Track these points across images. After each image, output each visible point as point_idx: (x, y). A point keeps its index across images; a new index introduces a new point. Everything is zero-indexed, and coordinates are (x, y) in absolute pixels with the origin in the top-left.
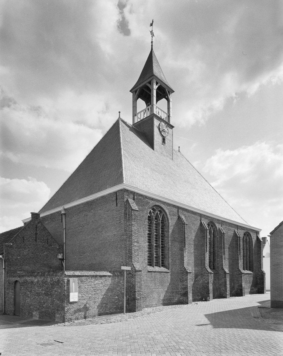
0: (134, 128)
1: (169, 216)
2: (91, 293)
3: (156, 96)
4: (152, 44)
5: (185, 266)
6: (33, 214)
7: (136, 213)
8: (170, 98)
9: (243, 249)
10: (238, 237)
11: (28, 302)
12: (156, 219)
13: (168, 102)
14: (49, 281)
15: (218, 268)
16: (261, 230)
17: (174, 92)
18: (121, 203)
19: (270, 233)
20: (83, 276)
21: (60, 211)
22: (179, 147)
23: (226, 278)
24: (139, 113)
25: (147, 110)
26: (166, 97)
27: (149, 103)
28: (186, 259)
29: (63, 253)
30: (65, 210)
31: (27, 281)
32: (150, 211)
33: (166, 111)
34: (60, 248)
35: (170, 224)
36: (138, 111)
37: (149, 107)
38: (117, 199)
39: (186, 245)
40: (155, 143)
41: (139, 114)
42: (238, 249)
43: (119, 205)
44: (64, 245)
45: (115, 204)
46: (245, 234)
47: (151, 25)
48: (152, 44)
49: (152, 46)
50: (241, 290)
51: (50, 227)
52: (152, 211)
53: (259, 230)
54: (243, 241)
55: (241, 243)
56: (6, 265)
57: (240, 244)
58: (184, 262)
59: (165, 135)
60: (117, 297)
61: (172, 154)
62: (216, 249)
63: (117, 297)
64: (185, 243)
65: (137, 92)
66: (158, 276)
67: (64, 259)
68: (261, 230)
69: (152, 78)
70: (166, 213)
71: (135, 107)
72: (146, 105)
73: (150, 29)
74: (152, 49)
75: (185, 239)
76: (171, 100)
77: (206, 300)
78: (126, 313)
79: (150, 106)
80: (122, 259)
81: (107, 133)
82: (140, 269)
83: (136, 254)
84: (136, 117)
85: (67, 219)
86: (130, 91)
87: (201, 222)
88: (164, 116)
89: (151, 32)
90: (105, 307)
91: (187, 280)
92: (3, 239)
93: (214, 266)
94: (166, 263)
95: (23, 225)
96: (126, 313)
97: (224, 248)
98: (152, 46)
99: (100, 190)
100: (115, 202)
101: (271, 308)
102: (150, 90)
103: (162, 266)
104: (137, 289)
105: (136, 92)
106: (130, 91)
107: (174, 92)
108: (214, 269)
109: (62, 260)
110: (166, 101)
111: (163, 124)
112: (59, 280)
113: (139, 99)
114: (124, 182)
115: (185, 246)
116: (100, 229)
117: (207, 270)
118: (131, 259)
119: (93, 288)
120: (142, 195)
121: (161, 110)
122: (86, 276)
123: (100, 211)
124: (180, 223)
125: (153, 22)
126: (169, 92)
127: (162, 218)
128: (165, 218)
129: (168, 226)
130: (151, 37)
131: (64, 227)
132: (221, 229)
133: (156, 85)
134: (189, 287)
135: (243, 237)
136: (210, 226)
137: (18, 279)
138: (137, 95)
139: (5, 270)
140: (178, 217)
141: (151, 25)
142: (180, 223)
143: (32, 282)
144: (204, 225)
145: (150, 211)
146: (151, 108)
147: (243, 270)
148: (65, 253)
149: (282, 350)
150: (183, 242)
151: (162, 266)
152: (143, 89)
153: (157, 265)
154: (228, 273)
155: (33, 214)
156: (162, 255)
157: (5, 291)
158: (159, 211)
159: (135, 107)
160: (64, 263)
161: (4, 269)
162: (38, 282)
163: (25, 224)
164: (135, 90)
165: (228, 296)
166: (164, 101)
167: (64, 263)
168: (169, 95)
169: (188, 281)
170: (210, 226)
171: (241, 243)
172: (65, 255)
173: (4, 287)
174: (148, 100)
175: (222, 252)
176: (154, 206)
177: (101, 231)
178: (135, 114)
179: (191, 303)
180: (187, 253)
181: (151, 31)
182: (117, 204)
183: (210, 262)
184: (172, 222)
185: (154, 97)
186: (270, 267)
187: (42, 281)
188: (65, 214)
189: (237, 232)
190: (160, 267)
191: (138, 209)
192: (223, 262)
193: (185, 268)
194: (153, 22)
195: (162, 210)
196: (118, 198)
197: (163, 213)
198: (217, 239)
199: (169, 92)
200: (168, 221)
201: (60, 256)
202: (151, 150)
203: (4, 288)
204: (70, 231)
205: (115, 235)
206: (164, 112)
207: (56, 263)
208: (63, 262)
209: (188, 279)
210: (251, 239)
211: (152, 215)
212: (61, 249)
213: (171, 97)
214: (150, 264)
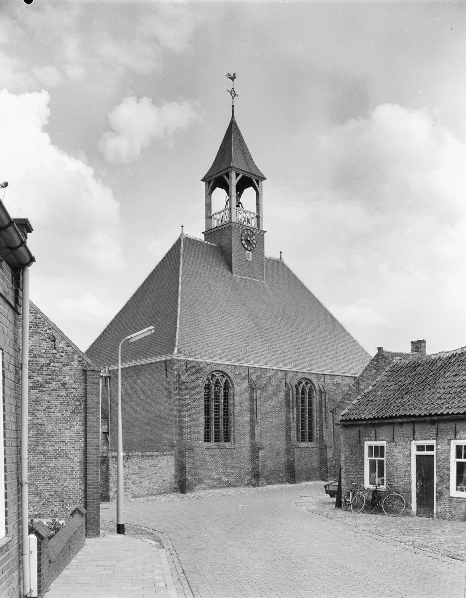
1: (233, 381)
4: (233, 109)
22: (281, 252)
36: (213, 212)
43: (169, 376)
48: (233, 109)
49: (233, 111)
71: (209, 206)
74: (233, 117)
98: (233, 111)
99: (378, 472)
105: (209, 182)
118: (182, 436)
126: (258, 182)
130: (232, 99)
149: (465, 501)
168: (259, 186)
176: (213, 372)
178: (209, 217)
188: (110, 377)
197: (226, 378)
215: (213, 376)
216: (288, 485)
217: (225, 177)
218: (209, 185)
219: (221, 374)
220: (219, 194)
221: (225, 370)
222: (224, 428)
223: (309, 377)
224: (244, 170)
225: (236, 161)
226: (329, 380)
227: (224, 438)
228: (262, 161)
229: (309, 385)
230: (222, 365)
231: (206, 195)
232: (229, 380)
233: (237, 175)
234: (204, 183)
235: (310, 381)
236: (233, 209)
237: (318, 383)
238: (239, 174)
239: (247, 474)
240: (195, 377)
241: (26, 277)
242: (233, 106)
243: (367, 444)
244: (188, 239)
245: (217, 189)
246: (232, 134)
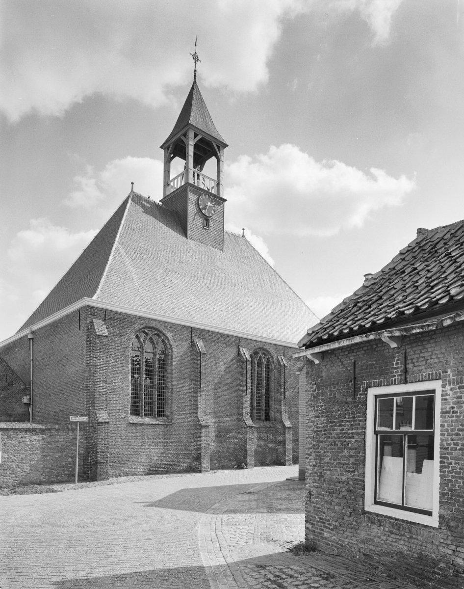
1: (172, 342)
2: (24, 453)
3: (193, 155)
4: (195, 74)
5: (199, 416)
7: (104, 340)
8: (220, 155)
13: (218, 162)
15: (275, 420)
17: (227, 146)
20: (12, 429)
21: (26, 336)
23: (285, 434)
28: (201, 406)
29: (30, 394)
30: (33, 332)
34: (27, 388)
35: (175, 354)
38: (80, 320)
40: (189, 228)
41: (172, 182)
44: (31, 383)
48: (195, 74)
49: (195, 76)
58: (197, 411)
59: (209, 214)
60: (70, 460)
61: (220, 240)
62: (272, 390)
63: (70, 460)
65: (170, 148)
66: (149, 430)
69: (186, 129)
70: (167, 338)
71: (167, 172)
75: (200, 375)
76: (222, 158)
77: (240, 467)
78: (78, 481)
80: (83, 406)
83: (104, 398)
84: (167, 189)
86: (161, 147)
90: (50, 472)
91: (200, 437)
94: (168, 412)
96: (78, 481)
97: (285, 388)
98: (195, 76)
104: (100, 448)
105: (168, 148)
107: (227, 146)
109: (28, 405)
115: (200, 386)
117: (245, 422)
118: (94, 406)
119: (27, 445)
120: (121, 313)
122: (16, 429)
124: (195, 354)
126: (219, 148)
129: (172, 357)
131: (32, 358)
134: (204, 447)
142: (195, 354)
148: (31, 395)
150: (197, 379)
153: (149, 414)
154: (289, 428)
164: (167, 145)
175: (281, 395)
178: (167, 184)
179: (207, 471)
181: (193, 53)
184: (178, 350)
185: (190, 157)
188: (33, 339)
191: (107, 335)
192: (283, 410)
199: (219, 148)
201: (25, 400)
204: (37, 363)
207: (20, 410)
209: (202, 435)
212: (26, 390)
213: (225, 154)
214: (135, 412)
217: (183, 138)
218: (168, 152)
220: (178, 164)
222: (159, 399)
223: (267, 347)
224: (204, 130)
225: (195, 119)
227: (159, 411)
228: (222, 129)
230: (156, 320)
233: (195, 136)
234: (163, 151)
235: (267, 351)
236: (189, 170)
238: (198, 135)
239: (187, 456)
240: (118, 332)
242: (195, 71)
243: (436, 385)
244: (137, 199)
245: (177, 158)
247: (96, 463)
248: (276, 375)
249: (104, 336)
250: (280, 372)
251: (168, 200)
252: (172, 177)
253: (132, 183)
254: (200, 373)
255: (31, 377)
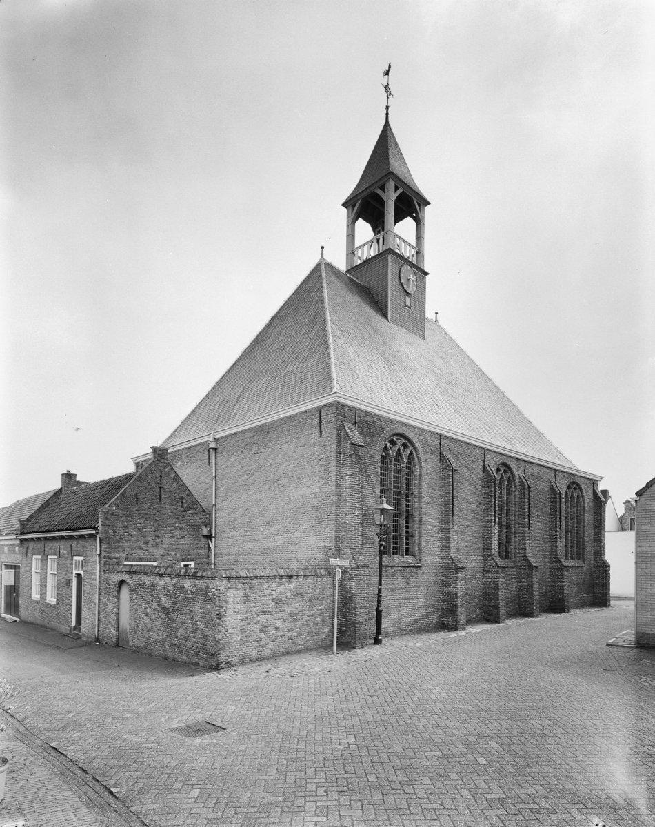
0: (350, 278)
1: (421, 454)
6: (155, 449)
9: (566, 518)
10: (555, 493)
11: (145, 623)
12: (396, 460)
13: (417, 226)
14: (187, 586)
16: (602, 478)
18: (330, 431)
19: (636, 494)
24: (359, 248)
25: (375, 242)
26: (414, 214)
27: (380, 228)
31: (144, 583)
32: (386, 446)
33: (413, 243)
37: (380, 236)
38: (321, 422)
39: (455, 513)
41: (360, 250)
42: (556, 518)
45: (318, 434)
46: (569, 487)
47: (387, 73)
49: (387, 114)
50: (562, 600)
51: (189, 474)
52: (389, 445)
53: (597, 479)
54: (566, 500)
55: (563, 505)
56: (103, 549)
57: (560, 508)
61: (417, 322)
64: (453, 507)
65: (358, 205)
67: (213, 535)
68: (602, 478)
71: (351, 235)
72: (374, 232)
73: (385, 80)
75: (453, 500)
79: (382, 233)
81: (297, 289)
82: (366, 563)
85: (218, 458)
86: (343, 205)
87: (484, 465)
88: (408, 252)
89: (386, 87)
92: (97, 495)
93: (507, 553)
95: (131, 469)
98: (387, 114)
100: (317, 429)
101: (637, 647)
102: (382, 202)
103: (406, 555)
106: (343, 205)
108: (507, 557)
110: (414, 223)
111: (406, 268)
112: (208, 587)
113: (360, 220)
114: (335, 390)
116: (285, 481)
121: (404, 241)
123: (285, 446)
125: (390, 67)
126: (419, 205)
127: (409, 459)
128: (413, 458)
129: (420, 475)
132: (522, 477)
133: (395, 191)
135: (566, 492)
136: (502, 472)
137: (126, 577)
138: (356, 212)
139: (100, 558)
140: (439, 457)
141: (387, 73)
143: (154, 586)
144: (490, 471)
145: (386, 446)
146: (383, 238)
147: (566, 558)
151: (406, 555)
152: (367, 201)
155: (155, 449)
156: (407, 532)
157: (99, 599)
158: (402, 445)
159: (351, 235)
160: (213, 543)
161: (99, 555)
162: (165, 586)
163: (138, 465)
165: (536, 613)
166: (408, 224)
167: (213, 543)
169: (459, 584)
170: (502, 472)
171: (563, 505)
172: (213, 529)
173: (97, 590)
174: (378, 223)
175: (525, 525)
176: (393, 435)
177: (288, 485)
180: (456, 528)
181: (385, 85)
182: (321, 432)
183: (500, 543)
186: (636, 563)
187: (174, 586)
188: (215, 449)
189: (554, 484)
190: (402, 555)
193: (452, 558)
194: (390, 67)
195: (408, 442)
196: (323, 421)
197: (411, 448)
198: (515, 497)
200: (420, 462)
202: (384, 320)
203: (97, 593)
205: (315, 494)
206: (409, 244)
208: (211, 541)
210: (581, 497)
211: (390, 454)
213: (428, 213)
215: (393, 442)
216: (487, 627)
217: (379, 192)
219: (404, 441)
221: (411, 436)
226: (530, 470)
228: (422, 181)
229: (509, 474)
230: (406, 425)
231: (348, 222)
232: (414, 453)
233: (397, 188)
234: (345, 210)
237: (517, 472)
241: (125, 672)
242: (387, 107)
244: (330, 267)
246: (385, 142)
247: (354, 623)
248: (517, 499)
249: (360, 446)
250: (522, 495)
251: (352, 270)
252: (358, 243)
253: (322, 248)
254: (453, 496)
255: (214, 500)
